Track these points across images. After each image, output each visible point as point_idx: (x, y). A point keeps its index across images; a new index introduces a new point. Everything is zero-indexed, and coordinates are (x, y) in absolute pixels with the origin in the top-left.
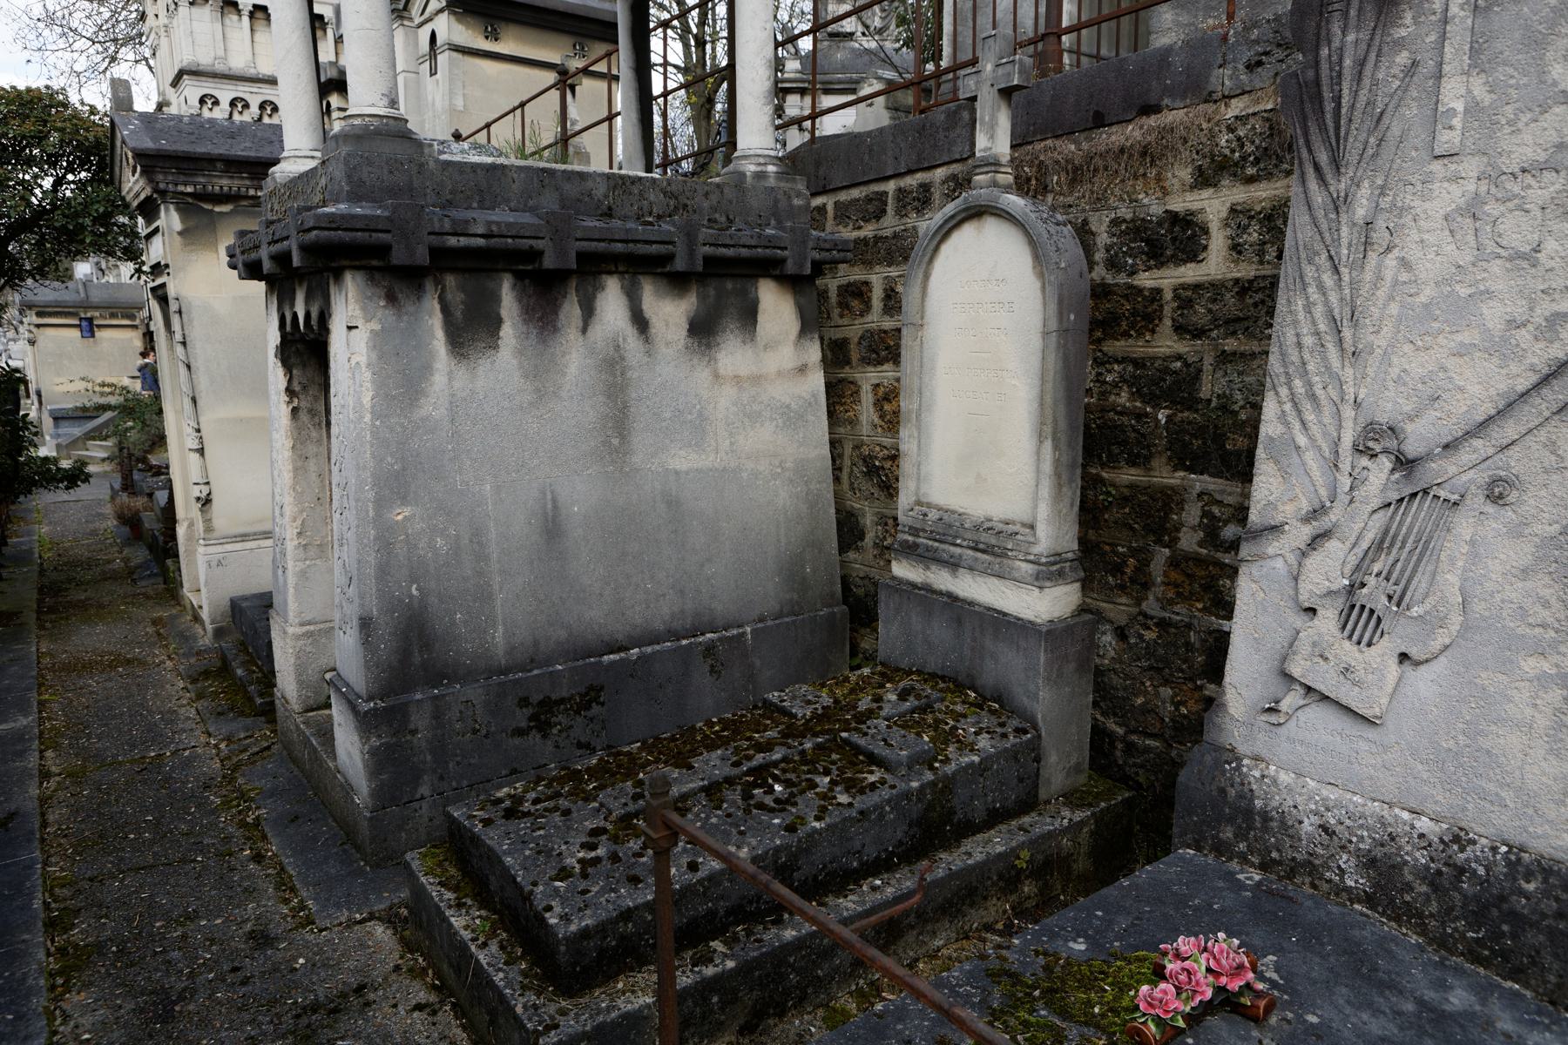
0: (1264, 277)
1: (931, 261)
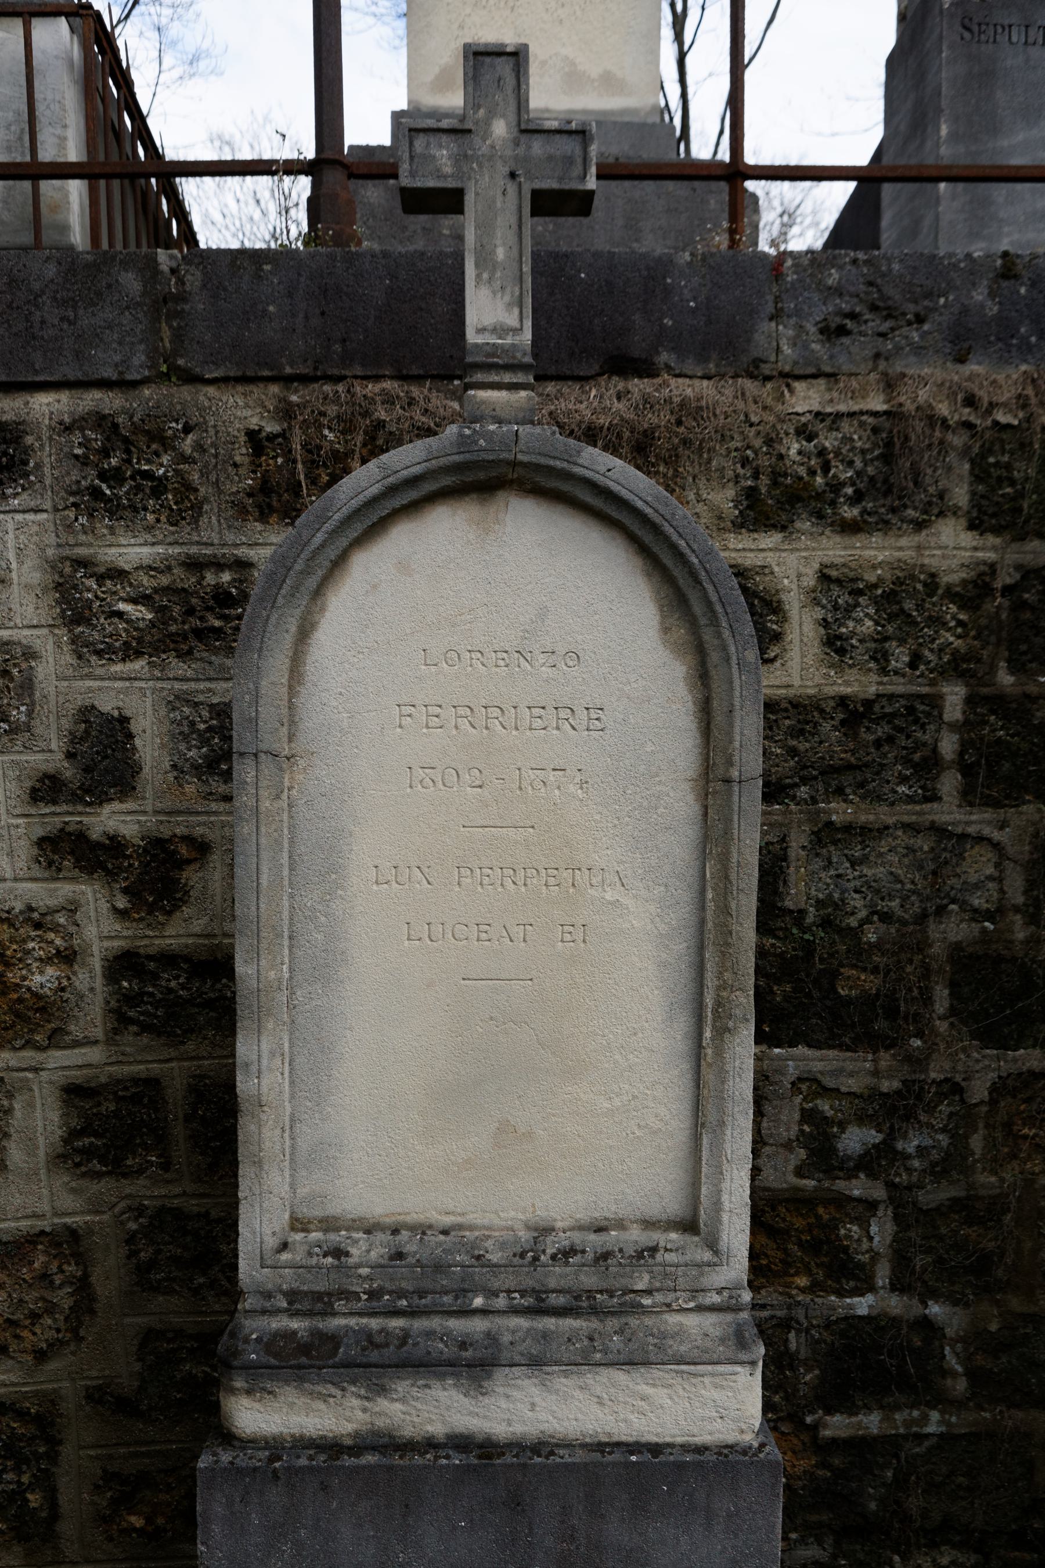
0: (891, 697)
1: (318, 593)
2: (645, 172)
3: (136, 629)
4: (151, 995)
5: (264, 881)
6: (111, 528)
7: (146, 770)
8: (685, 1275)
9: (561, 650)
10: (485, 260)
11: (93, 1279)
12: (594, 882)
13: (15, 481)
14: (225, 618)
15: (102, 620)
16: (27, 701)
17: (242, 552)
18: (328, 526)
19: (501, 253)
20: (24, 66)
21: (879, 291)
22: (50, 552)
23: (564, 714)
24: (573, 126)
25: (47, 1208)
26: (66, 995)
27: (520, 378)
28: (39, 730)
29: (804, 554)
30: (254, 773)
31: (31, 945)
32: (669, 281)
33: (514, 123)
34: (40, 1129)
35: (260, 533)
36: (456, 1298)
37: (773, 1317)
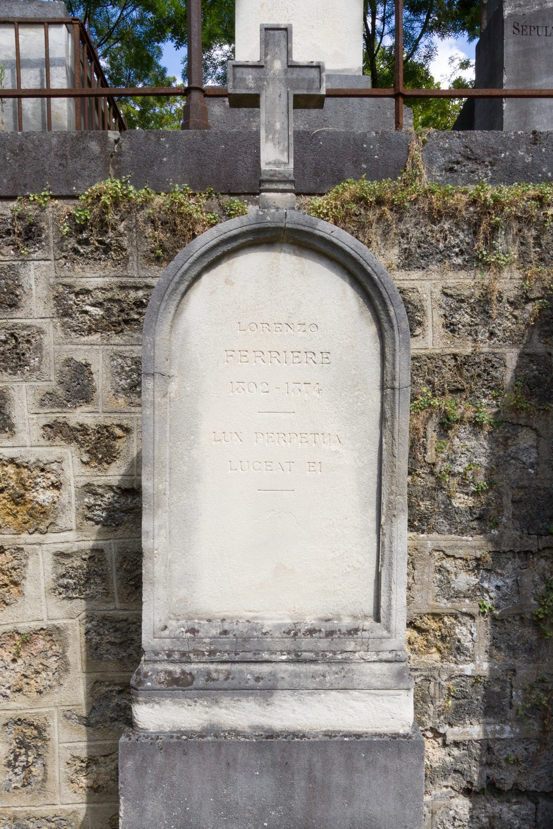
2: (353, 93)
3: (95, 320)
4: (100, 506)
5: (157, 438)
6: (83, 268)
7: (99, 391)
8: (373, 643)
9: (308, 323)
10: (270, 129)
11: (67, 654)
12: (325, 441)
13: (35, 245)
14: (140, 314)
15: (77, 315)
16: (39, 355)
17: (149, 281)
18: (191, 260)
19: (278, 126)
20: (44, 49)
21: (471, 150)
22: (52, 280)
23: (310, 355)
24: (314, 64)
25: (45, 617)
26: (56, 506)
27: (288, 187)
28: (44, 369)
29: (433, 282)
30: (152, 384)
31: (39, 480)
32: (365, 146)
33: (285, 62)
34: (42, 575)
35: (158, 271)
36: (255, 654)
37: (421, 675)
